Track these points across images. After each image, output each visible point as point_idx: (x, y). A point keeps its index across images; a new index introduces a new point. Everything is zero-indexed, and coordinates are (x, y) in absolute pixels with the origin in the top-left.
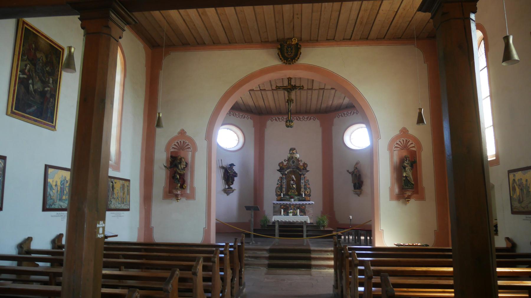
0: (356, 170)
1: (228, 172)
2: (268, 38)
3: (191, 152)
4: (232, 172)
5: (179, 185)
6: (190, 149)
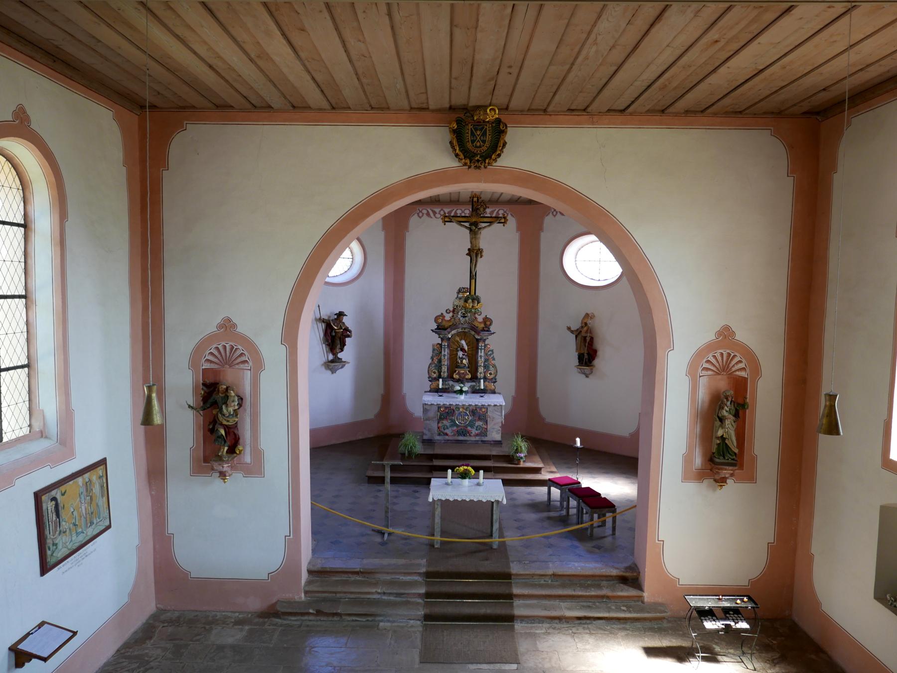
0: (585, 329)
1: (333, 329)
2: (427, 103)
3: (249, 372)
4: (342, 329)
5: (226, 448)
6: (246, 365)
